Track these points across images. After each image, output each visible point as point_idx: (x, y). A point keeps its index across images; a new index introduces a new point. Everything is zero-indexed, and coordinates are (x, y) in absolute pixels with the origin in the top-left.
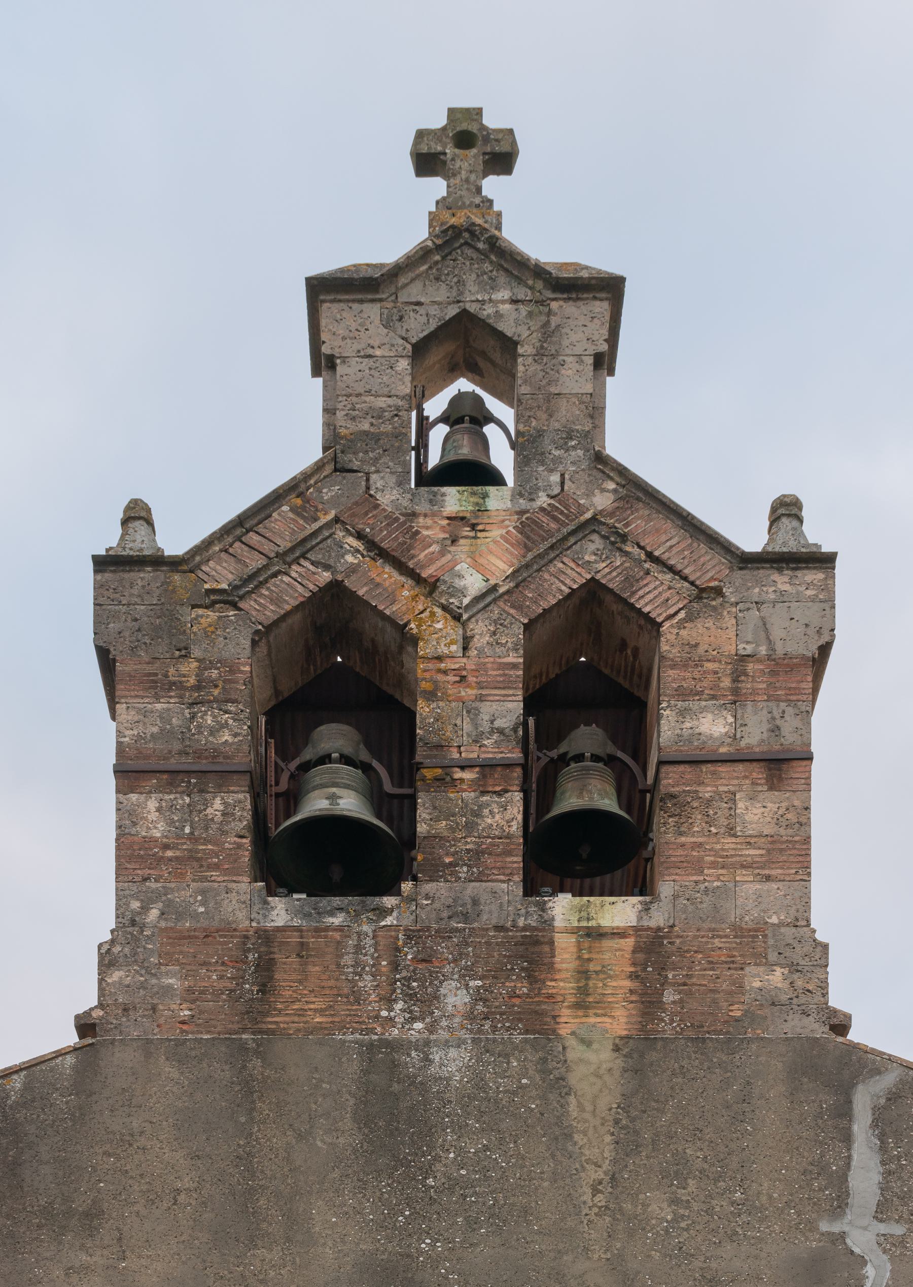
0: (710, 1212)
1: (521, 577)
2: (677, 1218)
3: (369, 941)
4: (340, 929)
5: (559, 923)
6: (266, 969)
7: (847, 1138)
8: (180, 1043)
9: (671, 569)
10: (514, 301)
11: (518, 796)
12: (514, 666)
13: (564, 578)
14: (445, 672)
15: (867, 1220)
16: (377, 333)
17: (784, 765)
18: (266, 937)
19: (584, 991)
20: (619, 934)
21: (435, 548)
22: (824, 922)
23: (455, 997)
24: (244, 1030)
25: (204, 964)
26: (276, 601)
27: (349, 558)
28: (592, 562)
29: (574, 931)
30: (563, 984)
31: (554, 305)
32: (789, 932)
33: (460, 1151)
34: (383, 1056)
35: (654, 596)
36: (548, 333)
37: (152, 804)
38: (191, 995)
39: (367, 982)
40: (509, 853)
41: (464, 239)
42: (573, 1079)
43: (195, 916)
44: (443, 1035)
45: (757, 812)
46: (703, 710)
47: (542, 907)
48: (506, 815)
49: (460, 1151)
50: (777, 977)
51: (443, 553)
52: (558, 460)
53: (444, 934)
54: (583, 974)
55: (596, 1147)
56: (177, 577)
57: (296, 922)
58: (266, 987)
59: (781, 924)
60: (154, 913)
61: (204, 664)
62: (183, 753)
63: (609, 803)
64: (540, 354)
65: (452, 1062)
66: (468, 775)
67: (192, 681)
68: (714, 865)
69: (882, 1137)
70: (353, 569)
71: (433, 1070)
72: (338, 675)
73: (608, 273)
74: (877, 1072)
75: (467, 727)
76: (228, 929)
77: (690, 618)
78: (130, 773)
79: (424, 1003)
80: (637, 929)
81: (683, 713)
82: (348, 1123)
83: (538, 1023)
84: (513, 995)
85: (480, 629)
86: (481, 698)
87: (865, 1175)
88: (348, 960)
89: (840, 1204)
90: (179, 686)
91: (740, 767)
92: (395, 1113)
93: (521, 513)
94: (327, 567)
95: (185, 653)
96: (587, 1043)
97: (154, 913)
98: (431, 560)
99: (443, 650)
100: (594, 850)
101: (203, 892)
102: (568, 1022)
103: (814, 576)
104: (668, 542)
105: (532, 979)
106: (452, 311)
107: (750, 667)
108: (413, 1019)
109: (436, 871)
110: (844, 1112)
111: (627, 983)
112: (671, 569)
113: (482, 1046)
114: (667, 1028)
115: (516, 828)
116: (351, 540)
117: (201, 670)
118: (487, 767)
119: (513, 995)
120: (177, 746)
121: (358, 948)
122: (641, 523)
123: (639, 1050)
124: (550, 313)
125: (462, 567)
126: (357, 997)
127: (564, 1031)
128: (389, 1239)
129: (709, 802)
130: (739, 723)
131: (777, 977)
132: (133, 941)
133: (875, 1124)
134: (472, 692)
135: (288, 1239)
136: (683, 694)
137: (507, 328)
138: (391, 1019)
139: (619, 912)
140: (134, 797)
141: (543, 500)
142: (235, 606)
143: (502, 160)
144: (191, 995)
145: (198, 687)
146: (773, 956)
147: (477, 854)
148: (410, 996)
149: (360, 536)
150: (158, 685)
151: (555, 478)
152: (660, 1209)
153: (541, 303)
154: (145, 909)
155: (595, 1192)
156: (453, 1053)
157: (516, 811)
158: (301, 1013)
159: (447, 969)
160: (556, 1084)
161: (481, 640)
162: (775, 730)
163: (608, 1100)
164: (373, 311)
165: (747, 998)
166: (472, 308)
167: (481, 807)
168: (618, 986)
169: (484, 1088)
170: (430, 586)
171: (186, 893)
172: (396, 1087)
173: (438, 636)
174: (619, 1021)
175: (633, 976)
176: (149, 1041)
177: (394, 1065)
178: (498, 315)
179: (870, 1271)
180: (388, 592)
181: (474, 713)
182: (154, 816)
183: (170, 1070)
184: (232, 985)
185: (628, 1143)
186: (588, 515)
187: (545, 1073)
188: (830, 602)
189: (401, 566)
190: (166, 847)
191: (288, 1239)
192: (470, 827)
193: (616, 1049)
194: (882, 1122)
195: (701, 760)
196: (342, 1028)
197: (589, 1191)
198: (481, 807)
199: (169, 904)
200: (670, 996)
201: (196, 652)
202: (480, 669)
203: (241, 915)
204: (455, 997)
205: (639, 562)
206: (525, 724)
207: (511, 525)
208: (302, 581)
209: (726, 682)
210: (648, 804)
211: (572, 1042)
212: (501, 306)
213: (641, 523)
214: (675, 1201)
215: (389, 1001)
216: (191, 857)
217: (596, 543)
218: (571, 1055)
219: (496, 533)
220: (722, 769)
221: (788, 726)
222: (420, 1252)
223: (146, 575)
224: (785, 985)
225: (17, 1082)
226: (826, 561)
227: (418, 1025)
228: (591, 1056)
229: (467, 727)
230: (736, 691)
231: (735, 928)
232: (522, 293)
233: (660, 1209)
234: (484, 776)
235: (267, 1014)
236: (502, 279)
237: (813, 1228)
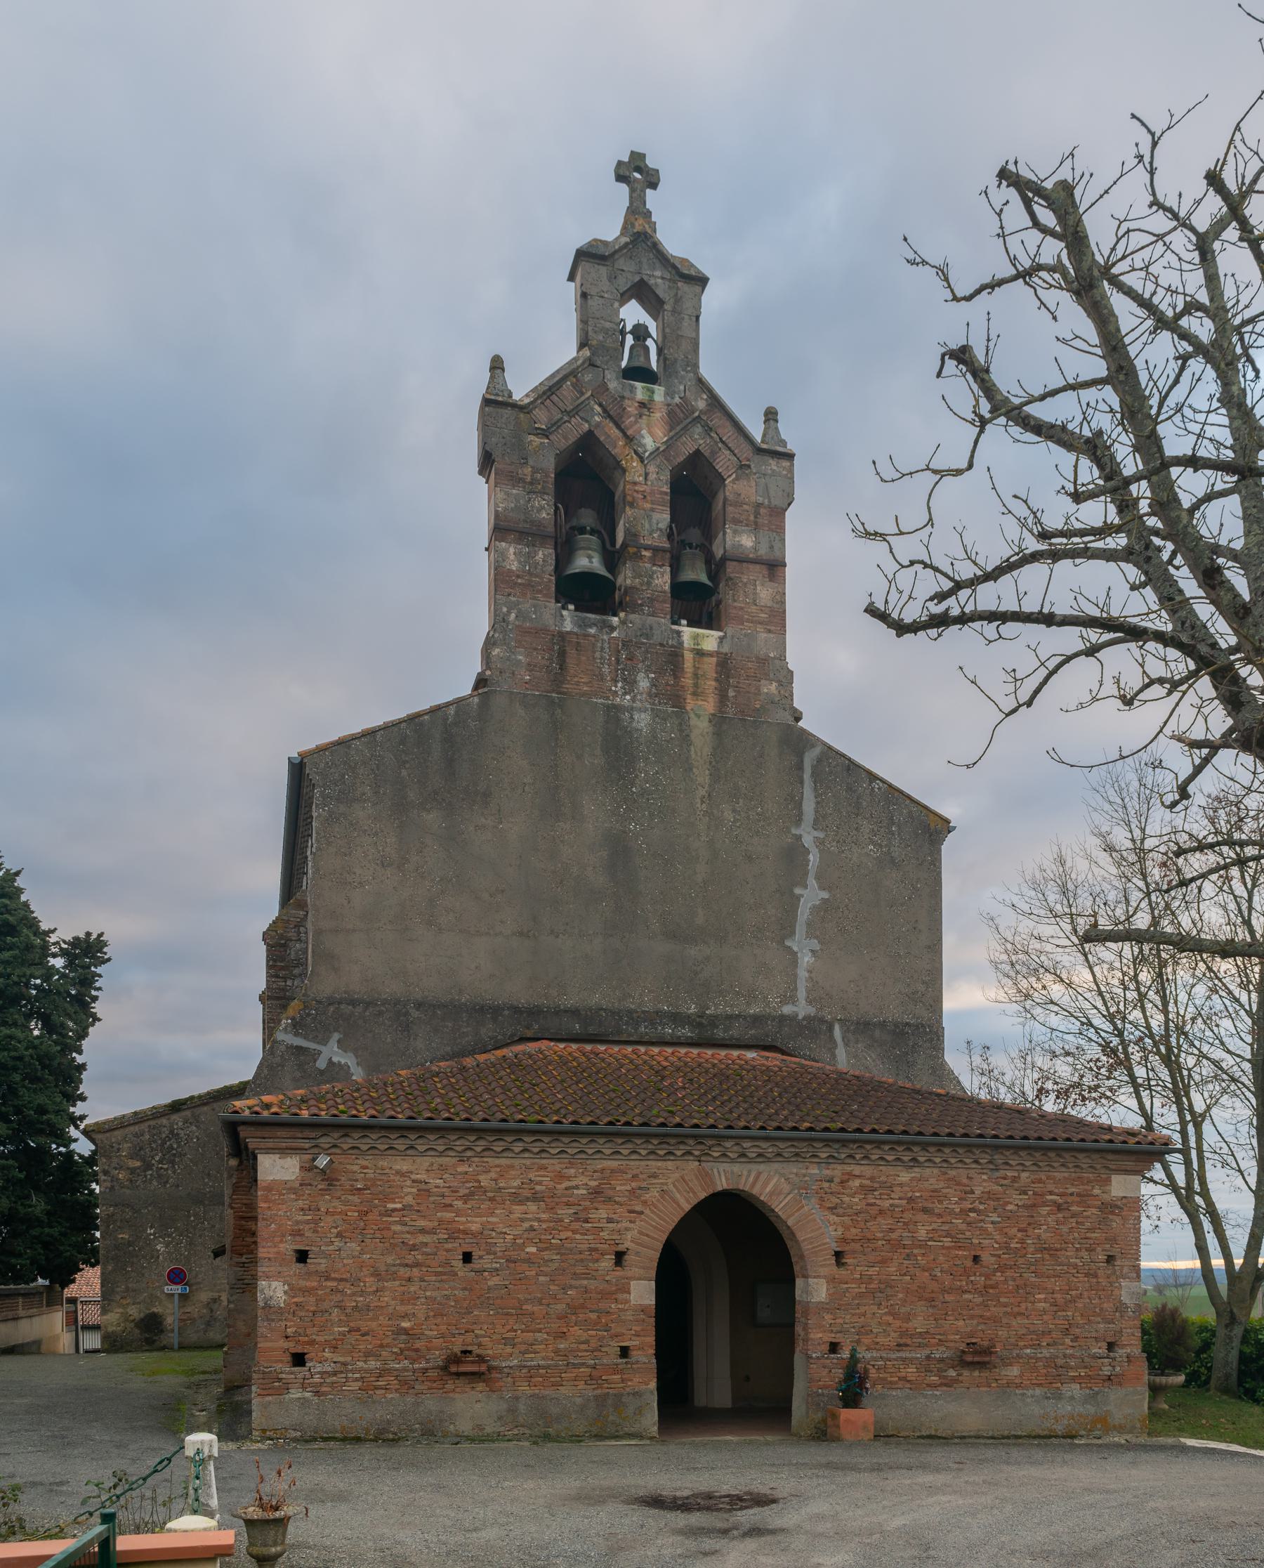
0: (748, 818)
1: (669, 444)
2: (736, 821)
3: (606, 645)
4: (594, 636)
5: (686, 645)
6: (562, 654)
7: (802, 782)
8: (525, 695)
9: (729, 449)
10: (663, 278)
11: (668, 569)
12: (666, 493)
13: (686, 448)
14: (637, 492)
15: (810, 829)
16: (605, 285)
17: (775, 567)
18: (562, 636)
19: (696, 685)
20: (710, 654)
21: (632, 419)
22: (792, 661)
23: (644, 684)
24: (553, 691)
25: (536, 649)
26: (566, 438)
27: (597, 418)
28: (695, 440)
29: (692, 650)
30: (688, 681)
31: (680, 284)
32: (777, 662)
33: (647, 773)
34: (613, 712)
35: (724, 462)
36: (678, 300)
37: (512, 550)
38: (531, 667)
39: (606, 669)
40: (664, 602)
41: (640, 237)
42: (693, 736)
43: (531, 620)
44: (638, 704)
45: (764, 593)
46: (743, 531)
47: (1052, 190)
48: (663, 580)
49: (647, 773)
50: (773, 687)
51: (636, 422)
52: (683, 377)
53: (639, 645)
54: (696, 675)
55: (702, 776)
56: (522, 415)
57: (576, 630)
58: (562, 666)
59: (774, 658)
60: (513, 616)
61: (535, 470)
62: (525, 521)
63: (704, 578)
64: (674, 311)
65: (642, 721)
66: (647, 554)
67: (529, 479)
68: (748, 621)
69: (815, 782)
70: (598, 425)
71: (634, 724)
72: (586, 480)
73: (699, 272)
74: (813, 746)
75: (647, 526)
76: (545, 630)
77: (737, 479)
78: (501, 530)
79: (630, 684)
80: (718, 653)
81: (735, 532)
82: (598, 752)
83: (677, 700)
84: (667, 684)
85: (652, 469)
86: (652, 510)
87: (809, 806)
88: (597, 655)
89: (799, 821)
90: (521, 480)
91: (758, 566)
92: (618, 747)
93: (669, 405)
94: (587, 421)
95: (524, 460)
96: (698, 716)
97: (513, 616)
98: (631, 426)
99: (637, 479)
100: (697, 603)
101: (535, 606)
102: (690, 703)
103: (786, 464)
104: (728, 433)
105: (676, 677)
106: (637, 279)
107: (762, 511)
108: (625, 694)
109: (634, 608)
110: (800, 767)
111: (713, 683)
112: (729, 449)
113: (656, 714)
114: (731, 711)
115: (667, 588)
116: (597, 407)
117: (533, 473)
118: (656, 550)
119: (667, 684)
120: (523, 517)
121: (602, 648)
122: (717, 420)
123: (719, 721)
124: (678, 288)
125: (644, 432)
126: (601, 678)
127: (688, 708)
128: (617, 821)
129: (745, 584)
130: (757, 542)
131: (773, 687)
132: (504, 631)
133: (812, 776)
134: (648, 506)
135: (573, 818)
136: (736, 521)
137: (660, 293)
138: (616, 692)
139: (710, 640)
140: (504, 544)
141: (677, 400)
142: (547, 437)
143: (654, 186)
144: (531, 667)
145: (531, 483)
146: (772, 675)
147: (652, 600)
148: (624, 680)
149: (600, 405)
150: (516, 480)
151: (682, 388)
152: (728, 815)
153: (675, 282)
154: (509, 612)
155: (703, 802)
156: (643, 716)
157: (667, 577)
158: (578, 683)
159: (640, 665)
160: (686, 739)
161: (652, 476)
162: (771, 547)
163: (707, 750)
164: (603, 271)
165: (762, 698)
166: (645, 278)
167: (654, 572)
168: (710, 685)
169: (655, 737)
170: (629, 439)
171: (526, 606)
172: (619, 733)
173: (635, 471)
174: (709, 705)
175: (716, 680)
176: (512, 693)
177: (618, 720)
178: (656, 284)
179: (811, 857)
180: (618, 447)
181: (650, 517)
182: (512, 557)
183: (521, 712)
184: (547, 663)
185: (716, 777)
186: (697, 414)
187: (681, 731)
188: (791, 480)
189: (618, 426)
190: (518, 577)
191: (573, 818)
192: (649, 583)
193: (710, 721)
194: (815, 774)
195: (742, 560)
196: (596, 695)
197: (699, 801)
198: (654, 572)
199: (519, 611)
200: (731, 693)
201: (531, 462)
202: (652, 493)
203: (551, 622)
204: (644, 684)
205: (716, 443)
206: (671, 528)
207: (664, 410)
208: (575, 429)
209: (752, 518)
210: (1191, 1442)
211: (692, 715)
212: (657, 279)
213: (717, 420)
214: (734, 811)
215: (615, 681)
216: (529, 585)
217: (698, 429)
218: (692, 723)
219: (658, 415)
220: (751, 566)
221: (777, 545)
222: (630, 830)
223: (507, 412)
224: (775, 692)
225: (452, 710)
226: (790, 456)
227: (628, 697)
228: (699, 723)
229: (647, 526)
230: (756, 523)
231: (757, 658)
232: (668, 276)
233: (728, 815)
234: (654, 555)
235: (562, 682)
236: (658, 265)
237: (789, 832)
